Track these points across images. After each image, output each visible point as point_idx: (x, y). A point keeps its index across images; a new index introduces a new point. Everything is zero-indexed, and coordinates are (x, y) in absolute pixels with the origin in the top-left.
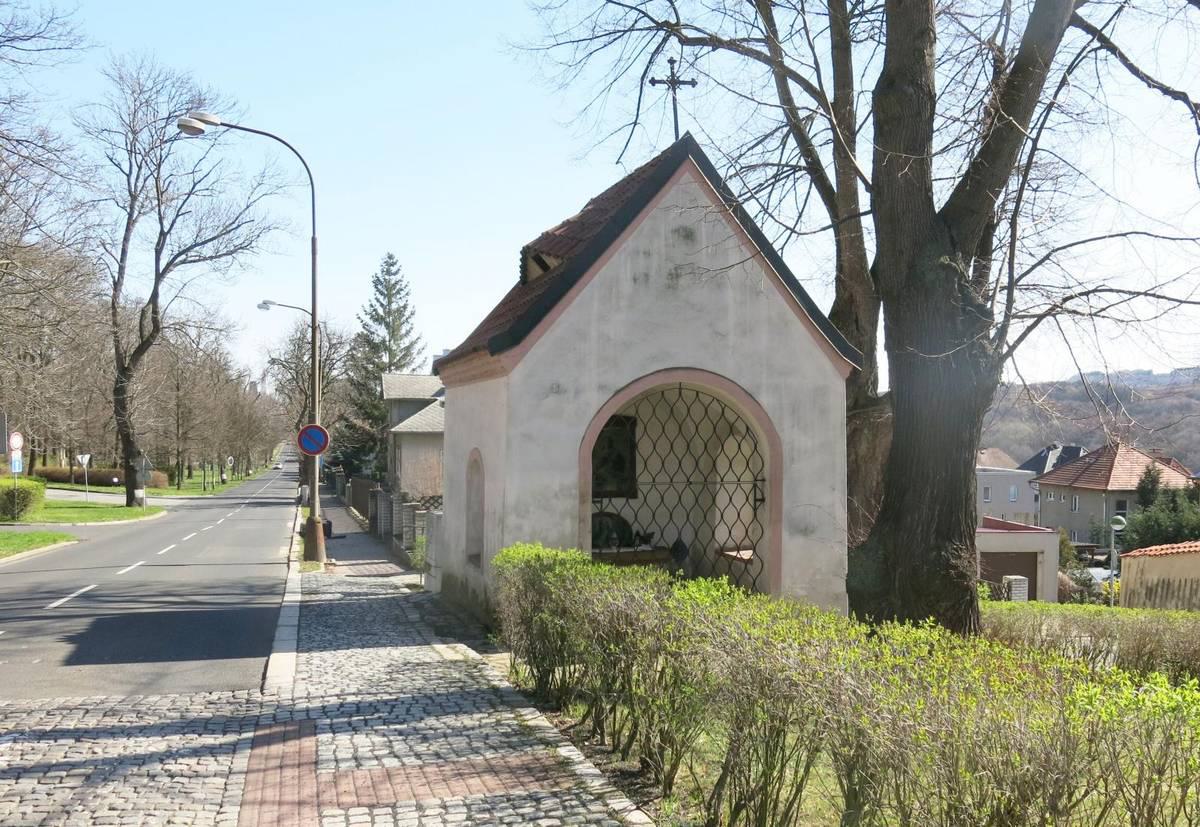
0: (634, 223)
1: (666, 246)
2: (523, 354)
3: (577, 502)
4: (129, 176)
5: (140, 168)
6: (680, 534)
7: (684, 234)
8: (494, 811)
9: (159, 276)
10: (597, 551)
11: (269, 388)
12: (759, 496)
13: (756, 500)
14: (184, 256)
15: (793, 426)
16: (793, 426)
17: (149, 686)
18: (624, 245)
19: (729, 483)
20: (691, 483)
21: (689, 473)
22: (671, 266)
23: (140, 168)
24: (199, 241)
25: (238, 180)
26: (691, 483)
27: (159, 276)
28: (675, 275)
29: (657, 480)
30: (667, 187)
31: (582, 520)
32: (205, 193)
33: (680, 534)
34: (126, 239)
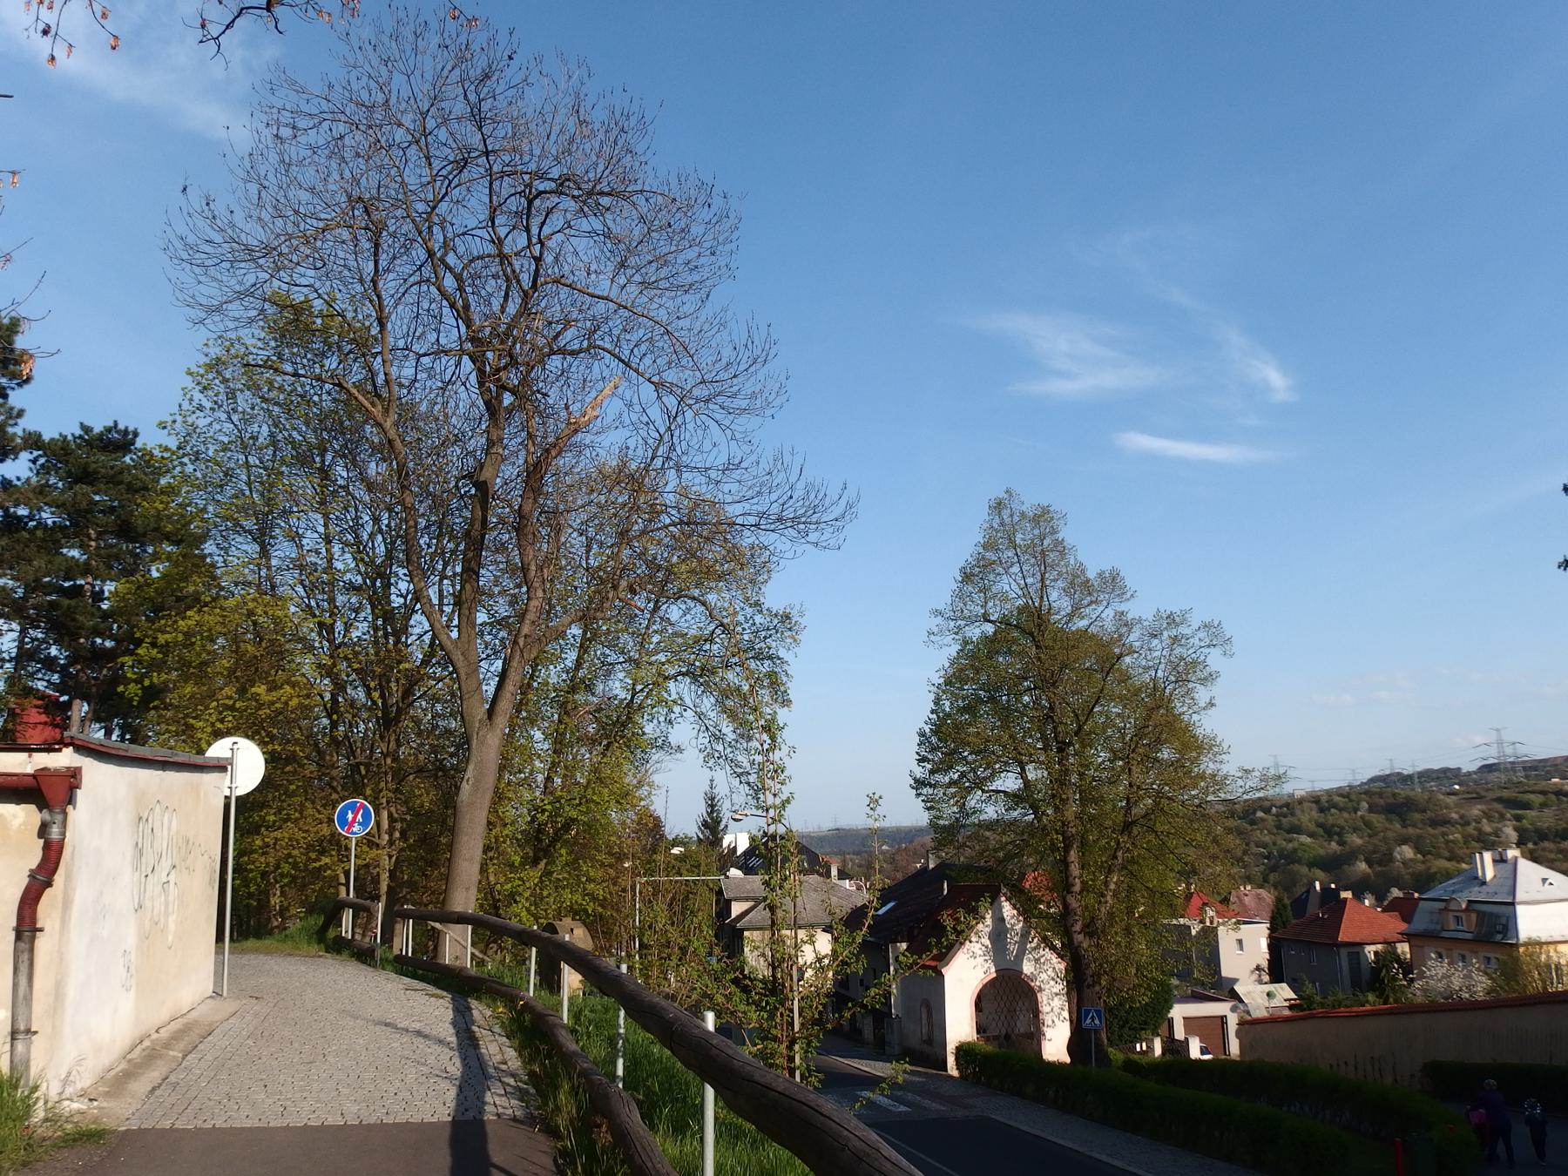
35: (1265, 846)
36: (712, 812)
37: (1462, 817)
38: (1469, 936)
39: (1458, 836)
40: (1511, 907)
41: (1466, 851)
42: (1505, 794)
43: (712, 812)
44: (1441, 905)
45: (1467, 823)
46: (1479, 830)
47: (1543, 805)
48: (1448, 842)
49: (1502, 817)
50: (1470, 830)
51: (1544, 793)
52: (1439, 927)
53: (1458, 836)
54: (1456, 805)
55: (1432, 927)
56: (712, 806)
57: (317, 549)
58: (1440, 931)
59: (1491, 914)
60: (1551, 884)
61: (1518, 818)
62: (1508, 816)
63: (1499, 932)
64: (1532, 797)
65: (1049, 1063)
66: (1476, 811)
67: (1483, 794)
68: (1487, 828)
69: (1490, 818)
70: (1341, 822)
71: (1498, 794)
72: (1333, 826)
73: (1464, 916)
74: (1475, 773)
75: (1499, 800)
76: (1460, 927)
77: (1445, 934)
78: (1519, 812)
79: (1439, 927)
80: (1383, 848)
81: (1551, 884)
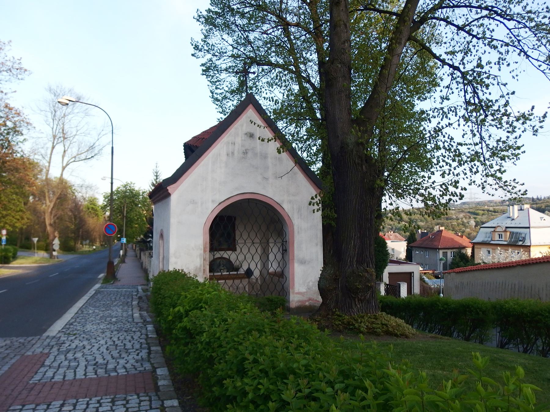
0: (227, 130)
1: (242, 140)
2: (178, 187)
3: (202, 252)
4: (53, 129)
5: (57, 125)
6: (249, 265)
7: (249, 135)
8: (139, 402)
9: (64, 168)
10: (212, 274)
11: (470, 256)
12: (284, 248)
13: (283, 250)
14: (75, 159)
15: (298, 218)
16: (298, 218)
17: (507, 257)
18: (223, 140)
19: (272, 243)
20: (254, 243)
21: (253, 239)
22: (244, 149)
23: (57, 125)
24: (79, 153)
25: (95, 128)
26: (254, 243)
27: (64, 168)
28: (245, 153)
29: (246, 242)
30: (242, 115)
31: (204, 260)
32: (83, 134)
33: (249, 265)
34: (51, 154)
35: (391, 225)
36: (157, 179)
37: (457, 217)
38: (506, 243)
39: (456, 223)
40: (528, 229)
41: (459, 228)
42: (471, 210)
43: (157, 179)
44: (493, 229)
45: (458, 219)
46: (463, 222)
47: (483, 214)
48: (452, 225)
49: (470, 218)
50: (460, 221)
51: (483, 210)
52: (490, 239)
53: (456, 223)
54: (455, 214)
55: (486, 239)
56: (157, 176)
57: (58, 120)
58: (490, 241)
59: (517, 233)
60: (544, 220)
61: (475, 218)
62: (472, 217)
63: (521, 241)
64: (480, 211)
65: (292, 308)
66: (461, 215)
67: (464, 210)
68: (465, 221)
69: (466, 218)
70: (417, 218)
71: (468, 210)
72: (414, 219)
73: (503, 234)
74: (459, 205)
75: (469, 212)
76: (501, 239)
77: (492, 242)
78: (475, 216)
79: (490, 239)
80: (431, 227)
81: (544, 220)
